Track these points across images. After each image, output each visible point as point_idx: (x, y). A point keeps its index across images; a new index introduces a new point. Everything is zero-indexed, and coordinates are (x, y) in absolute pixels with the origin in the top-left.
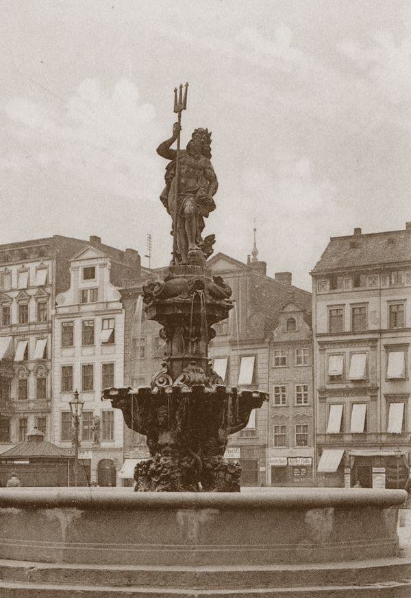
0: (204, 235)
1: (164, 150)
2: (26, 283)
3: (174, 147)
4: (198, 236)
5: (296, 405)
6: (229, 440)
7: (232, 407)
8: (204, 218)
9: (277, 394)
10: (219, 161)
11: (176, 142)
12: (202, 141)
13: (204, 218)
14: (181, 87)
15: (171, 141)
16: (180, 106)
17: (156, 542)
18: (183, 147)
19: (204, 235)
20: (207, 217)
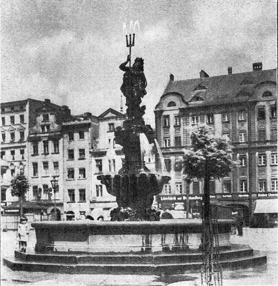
0: (141, 105)
1: (123, 67)
2: (115, 203)
3: (128, 65)
4: (138, 106)
5: (79, 140)
6: (109, 215)
7: (116, 187)
8: (141, 98)
9: (273, 184)
10: (147, 72)
11: (129, 63)
12: (140, 62)
13: (141, 98)
14: (130, 35)
15: (126, 63)
16: (130, 45)
17: (233, 182)
18: (132, 66)
19: (141, 105)
20: (143, 97)
